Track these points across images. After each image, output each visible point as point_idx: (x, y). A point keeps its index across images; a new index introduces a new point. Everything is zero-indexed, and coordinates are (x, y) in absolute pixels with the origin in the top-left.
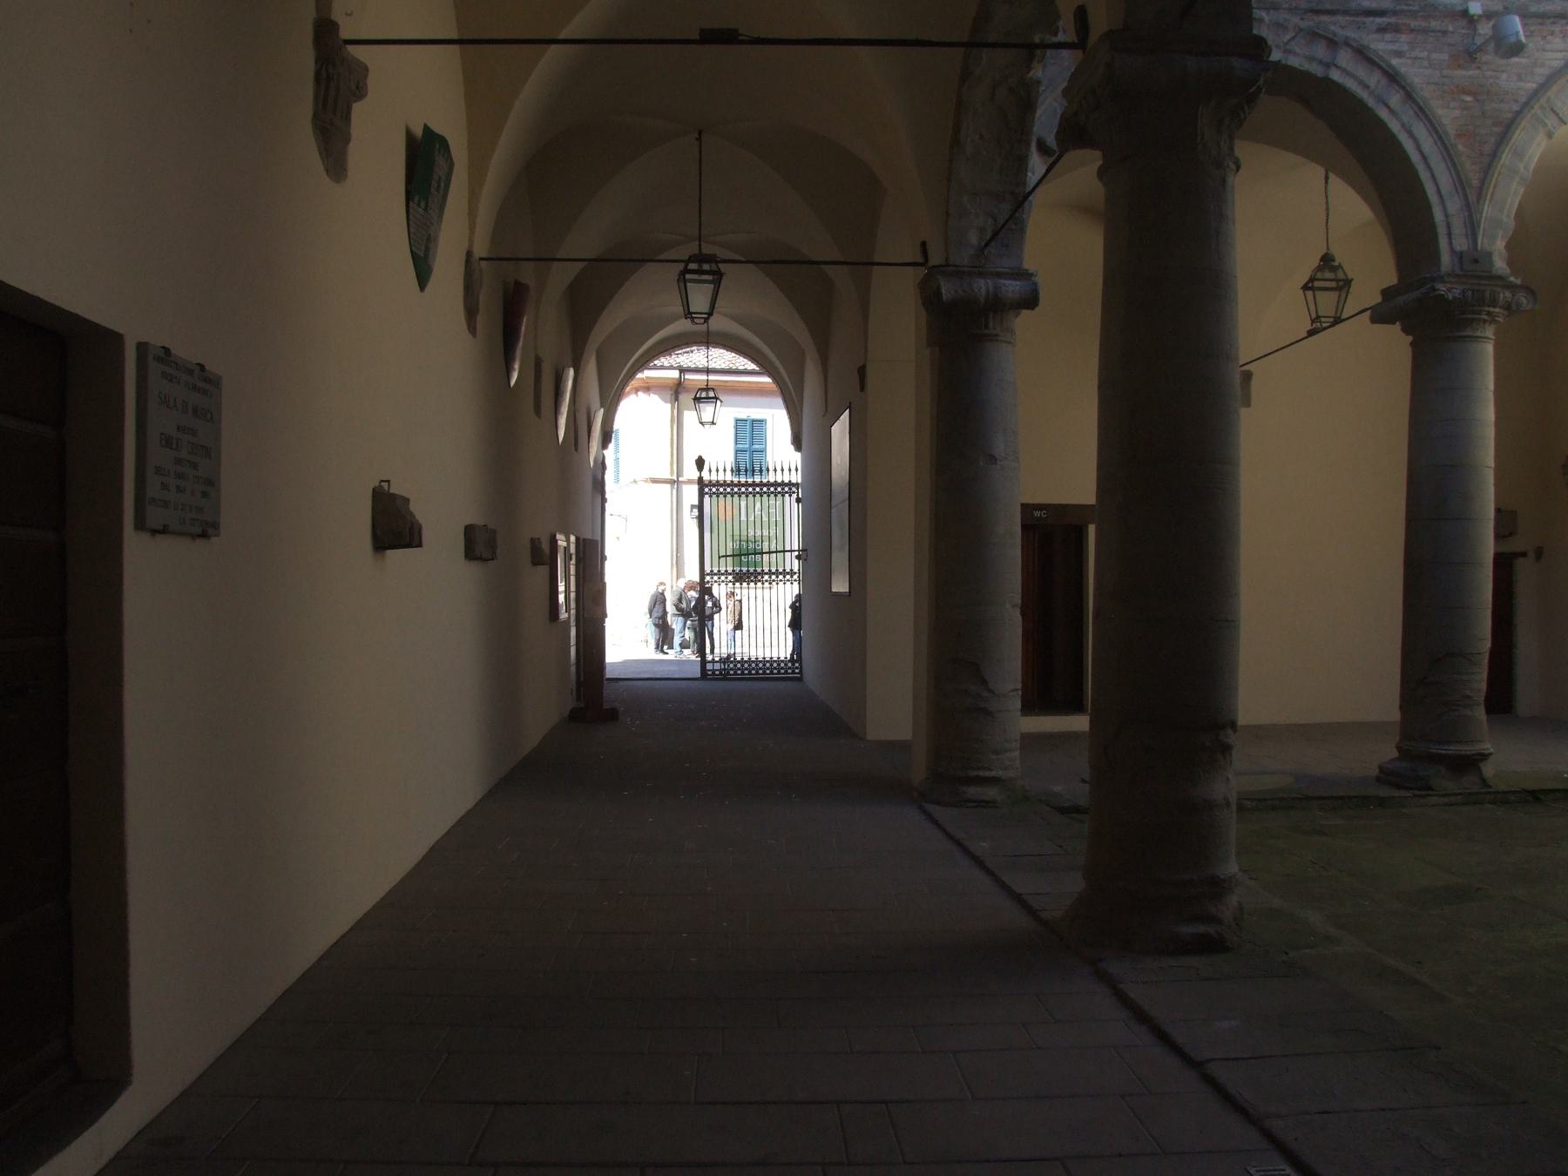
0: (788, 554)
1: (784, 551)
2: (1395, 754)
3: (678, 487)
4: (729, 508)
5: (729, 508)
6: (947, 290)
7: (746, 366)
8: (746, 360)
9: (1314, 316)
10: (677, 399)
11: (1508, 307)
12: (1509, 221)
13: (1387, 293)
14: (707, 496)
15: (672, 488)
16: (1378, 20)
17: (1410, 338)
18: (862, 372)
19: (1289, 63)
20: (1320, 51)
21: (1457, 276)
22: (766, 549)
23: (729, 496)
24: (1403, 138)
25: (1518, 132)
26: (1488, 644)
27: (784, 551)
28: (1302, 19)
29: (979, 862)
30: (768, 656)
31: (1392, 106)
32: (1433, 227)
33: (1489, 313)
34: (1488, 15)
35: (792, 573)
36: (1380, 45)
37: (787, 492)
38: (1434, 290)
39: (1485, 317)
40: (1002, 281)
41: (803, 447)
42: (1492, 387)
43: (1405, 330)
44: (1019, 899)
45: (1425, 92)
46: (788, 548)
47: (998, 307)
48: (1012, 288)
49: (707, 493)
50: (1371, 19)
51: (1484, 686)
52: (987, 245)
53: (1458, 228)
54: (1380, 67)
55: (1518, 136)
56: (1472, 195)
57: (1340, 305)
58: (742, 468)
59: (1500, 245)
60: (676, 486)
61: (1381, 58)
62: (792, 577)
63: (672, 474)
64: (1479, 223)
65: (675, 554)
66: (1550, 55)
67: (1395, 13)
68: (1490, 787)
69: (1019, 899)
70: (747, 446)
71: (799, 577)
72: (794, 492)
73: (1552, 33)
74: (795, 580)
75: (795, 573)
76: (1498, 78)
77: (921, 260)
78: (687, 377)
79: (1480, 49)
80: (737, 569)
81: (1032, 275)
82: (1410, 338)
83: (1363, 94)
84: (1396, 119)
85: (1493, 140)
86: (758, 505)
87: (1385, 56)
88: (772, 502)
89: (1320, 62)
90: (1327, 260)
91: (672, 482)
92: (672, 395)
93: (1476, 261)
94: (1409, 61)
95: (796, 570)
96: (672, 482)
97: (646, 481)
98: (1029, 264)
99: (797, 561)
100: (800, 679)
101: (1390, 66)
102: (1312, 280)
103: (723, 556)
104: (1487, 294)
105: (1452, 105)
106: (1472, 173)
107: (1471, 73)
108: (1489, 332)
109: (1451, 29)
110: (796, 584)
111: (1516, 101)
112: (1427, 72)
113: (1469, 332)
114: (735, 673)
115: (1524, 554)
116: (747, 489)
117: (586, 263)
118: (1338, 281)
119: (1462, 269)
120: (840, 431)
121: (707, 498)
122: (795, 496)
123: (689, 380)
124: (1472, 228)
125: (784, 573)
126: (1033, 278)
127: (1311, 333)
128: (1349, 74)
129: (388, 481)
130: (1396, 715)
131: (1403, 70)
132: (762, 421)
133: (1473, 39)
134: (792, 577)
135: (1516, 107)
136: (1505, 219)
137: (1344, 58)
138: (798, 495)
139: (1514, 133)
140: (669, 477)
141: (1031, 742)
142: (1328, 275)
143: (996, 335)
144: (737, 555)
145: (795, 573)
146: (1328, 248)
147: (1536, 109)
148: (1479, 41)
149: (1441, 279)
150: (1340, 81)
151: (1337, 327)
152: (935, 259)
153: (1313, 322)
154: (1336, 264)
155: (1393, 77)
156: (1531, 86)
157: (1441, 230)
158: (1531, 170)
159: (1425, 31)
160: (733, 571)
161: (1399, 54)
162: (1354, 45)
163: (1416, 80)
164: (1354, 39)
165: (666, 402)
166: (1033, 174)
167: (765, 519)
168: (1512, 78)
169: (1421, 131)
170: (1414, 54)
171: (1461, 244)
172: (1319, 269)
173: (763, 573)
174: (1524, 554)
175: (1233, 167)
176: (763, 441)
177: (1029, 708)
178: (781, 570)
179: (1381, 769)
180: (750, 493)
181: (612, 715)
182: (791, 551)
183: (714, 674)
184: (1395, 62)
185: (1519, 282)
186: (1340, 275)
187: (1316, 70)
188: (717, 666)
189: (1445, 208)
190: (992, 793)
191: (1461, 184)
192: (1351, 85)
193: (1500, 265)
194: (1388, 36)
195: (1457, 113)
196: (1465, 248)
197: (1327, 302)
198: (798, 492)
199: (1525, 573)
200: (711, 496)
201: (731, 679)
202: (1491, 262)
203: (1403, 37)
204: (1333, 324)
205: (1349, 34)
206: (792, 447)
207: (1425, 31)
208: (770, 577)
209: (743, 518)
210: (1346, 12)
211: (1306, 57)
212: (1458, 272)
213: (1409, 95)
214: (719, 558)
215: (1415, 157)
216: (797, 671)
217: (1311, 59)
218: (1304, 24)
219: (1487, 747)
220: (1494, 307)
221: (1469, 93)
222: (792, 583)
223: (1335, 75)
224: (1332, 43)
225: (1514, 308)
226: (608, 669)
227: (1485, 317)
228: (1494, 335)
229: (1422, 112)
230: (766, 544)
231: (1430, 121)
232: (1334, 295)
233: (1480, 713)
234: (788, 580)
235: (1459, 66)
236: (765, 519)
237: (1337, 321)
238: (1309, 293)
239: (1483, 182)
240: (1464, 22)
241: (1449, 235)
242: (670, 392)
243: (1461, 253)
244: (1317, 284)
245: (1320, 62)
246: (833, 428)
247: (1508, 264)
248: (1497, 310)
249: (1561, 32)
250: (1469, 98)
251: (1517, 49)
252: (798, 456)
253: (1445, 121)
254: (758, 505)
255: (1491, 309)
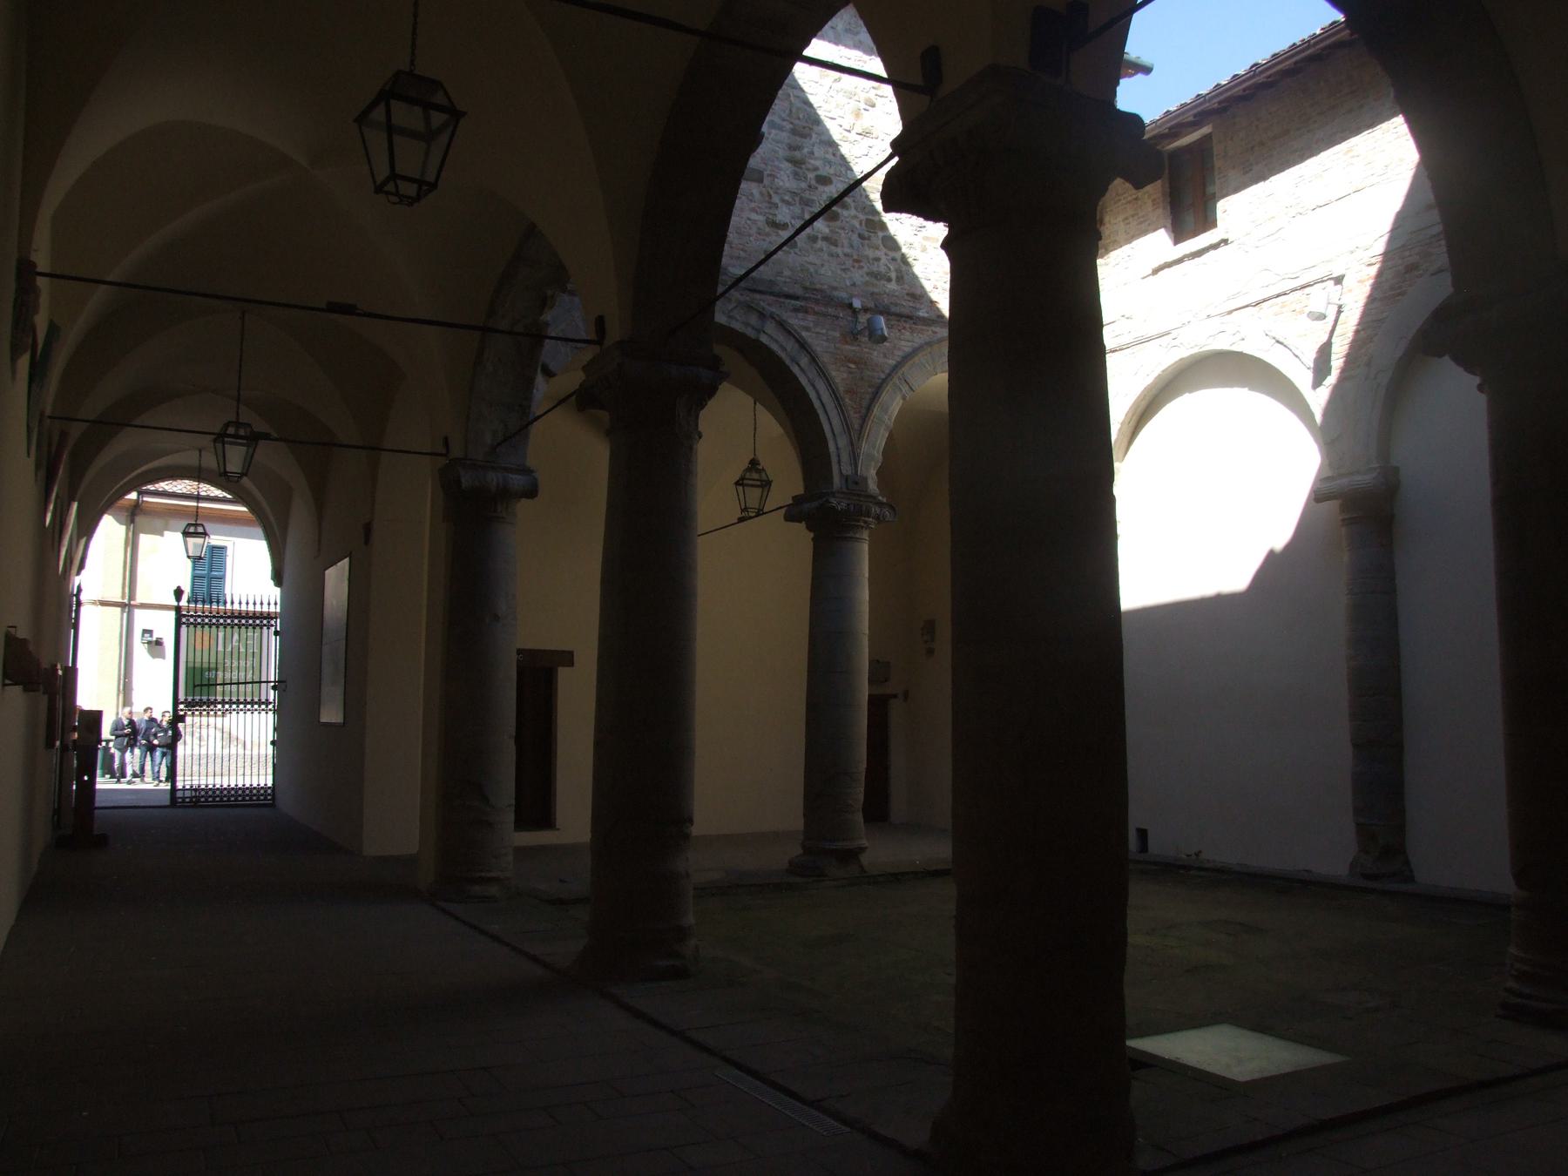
0: (264, 685)
1: (260, 682)
2: (800, 851)
3: (129, 612)
4: (206, 639)
5: (206, 639)
6: (467, 480)
7: (209, 493)
8: (208, 486)
9: (743, 507)
10: (132, 521)
11: (877, 518)
12: (878, 456)
13: (797, 500)
14: (184, 626)
15: (123, 612)
16: (793, 302)
17: (812, 535)
18: (368, 529)
19: (732, 326)
20: (754, 319)
21: (843, 493)
22: (235, 679)
23: (207, 626)
24: (809, 389)
25: (884, 393)
26: (865, 766)
27: (260, 682)
28: (742, 295)
29: (495, 938)
30: (195, 783)
31: (802, 365)
32: (829, 456)
33: (865, 522)
34: (865, 310)
35: (267, 703)
36: (794, 321)
37: (265, 625)
38: (827, 501)
39: (862, 524)
40: (511, 475)
41: (284, 584)
42: (867, 575)
43: (809, 528)
44: (534, 959)
45: (825, 359)
46: (264, 679)
47: (506, 495)
48: (517, 481)
49: (184, 623)
50: (789, 301)
51: (861, 797)
52: (499, 444)
53: (845, 457)
54: (794, 337)
55: (885, 396)
56: (855, 434)
57: (764, 499)
58: (200, 597)
59: (873, 472)
60: (127, 610)
61: (795, 331)
62: (267, 707)
63: (123, 597)
64: (859, 456)
65: (122, 677)
66: (903, 343)
67: (805, 299)
68: (865, 872)
69: (534, 959)
70: (206, 572)
71: (274, 707)
72: (272, 626)
73: (904, 328)
74: (270, 710)
75: (270, 703)
76: (871, 354)
77: (444, 451)
78: (145, 499)
79: (860, 332)
80: (190, 699)
81: (532, 471)
82: (812, 535)
83: (783, 355)
84: (805, 376)
85: (868, 397)
86: (236, 637)
87: (799, 330)
88: (250, 634)
89: (753, 328)
90: (754, 463)
91: (122, 605)
92: (127, 516)
93: (857, 483)
94: (814, 335)
95: (271, 700)
96: (122, 605)
97: (93, 603)
98: (531, 462)
99: (272, 692)
100: (273, 805)
101: (801, 337)
102: (742, 478)
103: (198, 685)
104: (864, 508)
105: (842, 369)
106: (856, 424)
107: (854, 348)
108: (865, 535)
109: (841, 315)
110: (271, 713)
111: (883, 372)
112: (825, 344)
113: (851, 534)
114: (206, 801)
115: (895, 696)
116: (240, 621)
117: (133, 423)
118: (761, 481)
119: (848, 489)
120: (336, 579)
121: (184, 629)
122: (273, 629)
123: (147, 502)
124: (854, 458)
125: (260, 703)
126: (534, 474)
127: (741, 520)
128: (772, 338)
129: (15, 627)
130: (799, 824)
131: (810, 340)
132: (223, 548)
133: (856, 325)
134: (267, 707)
135: (883, 376)
136: (876, 455)
137: (770, 327)
138: (276, 628)
139: (882, 393)
140: (120, 600)
141: (523, 852)
142: (755, 476)
143: (503, 518)
144: (213, 685)
145: (270, 703)
146: (755, 455)
147: (895, 379)
148: (860, 327)
149: (833, 494)
150: (767, 343)
151: (759, 518)
152: (456, 451)
153: (742, 511)
154: (760, 467)
155: (803, 345)
156: (892, 362)
157: (834, 459)
158: (893, 420)
159: (825, 315)
160: (186, 700)
161: (807, 329)
162: (777, 318)
163: (818, 349)
164: (777, 315)
165: (121, 523)
166: (537, 390)
167: (242, 650)
168: (880, 357)
169: (821, 386)
170: (818, 330)
171: (847, 470)
172: (748, 470)
173: (215, 703)
174: (895, 696)
175: (697, 437)
176: (222, 566)
177: (522, 824)
178: (256, 700)
179: (790, 862)
180: (250, 625)
181: (102, 841)
182: (268, 682)
183: (184, 801)
184: (804, 334)
185: (885, 500)
186: (764, 477)
187: (750, 333)
188: (188, 794)
189: (837, 444)
190: (493, 890)
191: (847, 426)
192: (774, 347)
193: (873, 486)
194: (800, 315)
195: (845, 375)
196: (850, 473)
197: (754, 495)
198: (276, 625)
199: (896, 713)
200: (188, 627)
201: (201, 806)
202: (867, 484)
203: (810, 318)
204: (756, 516)
205: (774, 310)
206: (272, 583)
207: (825, 315)
208: (230, 707)
209: (221, 648)
210: (772, 294)
211: (743, 323)
212: (844, 490)
213: (814, 359)
214: (195, 686)
215: (817, 404)
216: (269, 797)
217: (747, 324)
218: (742, 299)
219: (864, 842)
220: (869, 517)
221: (855, 363)
222: (267, 713)
223: (764, 339)
224: (762, 315)
225: (882, 519)
226: (97, 799)
227: (862, 524)
228: (869, 537)
229: (823, 373)
230: (220, 674)
231: (827, 379)
232: (758, 491)
233: (859, 817)
234: (263, 710)
235: (847, 343)
236: (242, 650)
237: (760, 513)
238: (740, 488)
239: (862, 426)
240: (850, 312)
241: (839, 462)
242: (126, 514)
243: (847, 476)
244: (745, 482)
245: (753, 328)
246: (327, 572)
247: (878, 487)
248: (871, 519)
249: (910, 328)
250: (853, 366)
251: (884, 339)
252: (278, 590)
253: (837, 380)
254: (236, 637)
255: (866, 519)
